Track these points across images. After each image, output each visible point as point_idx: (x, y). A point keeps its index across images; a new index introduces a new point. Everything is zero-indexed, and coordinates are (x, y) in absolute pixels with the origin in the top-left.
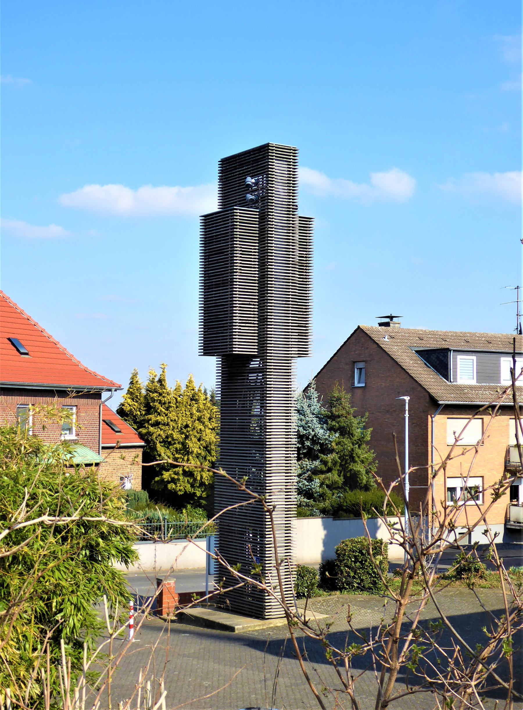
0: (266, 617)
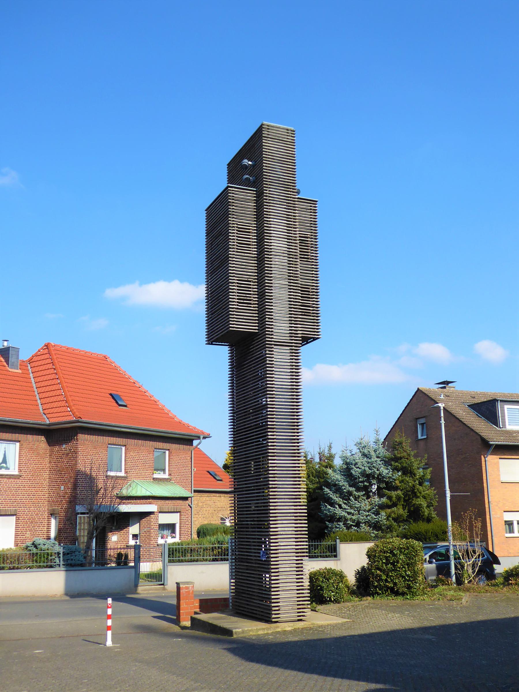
0: (274, 620)
